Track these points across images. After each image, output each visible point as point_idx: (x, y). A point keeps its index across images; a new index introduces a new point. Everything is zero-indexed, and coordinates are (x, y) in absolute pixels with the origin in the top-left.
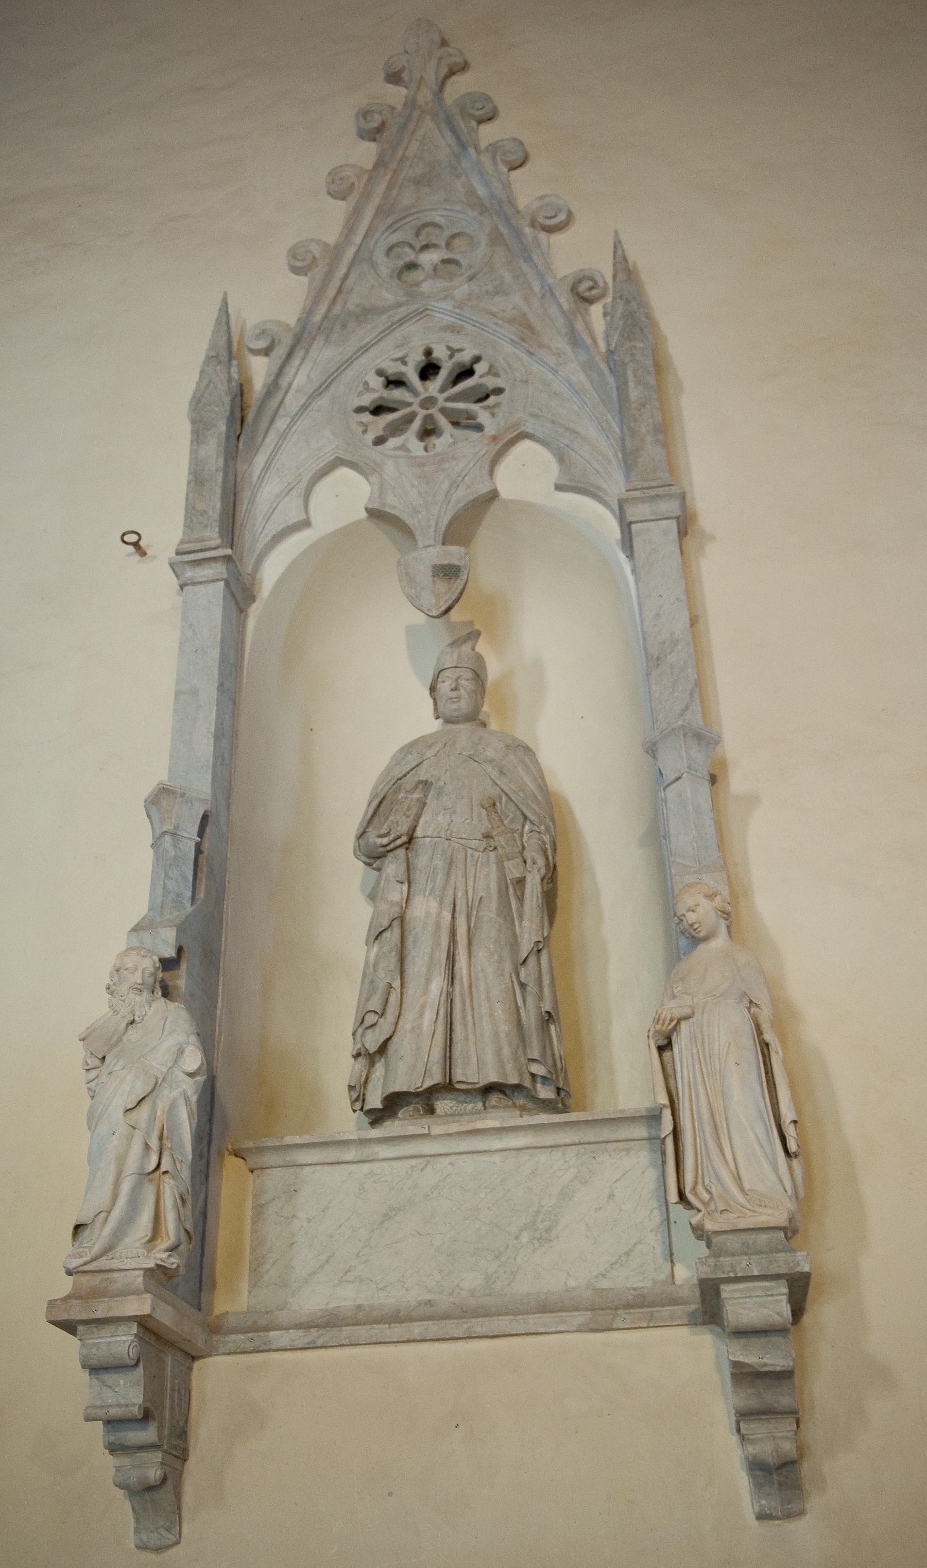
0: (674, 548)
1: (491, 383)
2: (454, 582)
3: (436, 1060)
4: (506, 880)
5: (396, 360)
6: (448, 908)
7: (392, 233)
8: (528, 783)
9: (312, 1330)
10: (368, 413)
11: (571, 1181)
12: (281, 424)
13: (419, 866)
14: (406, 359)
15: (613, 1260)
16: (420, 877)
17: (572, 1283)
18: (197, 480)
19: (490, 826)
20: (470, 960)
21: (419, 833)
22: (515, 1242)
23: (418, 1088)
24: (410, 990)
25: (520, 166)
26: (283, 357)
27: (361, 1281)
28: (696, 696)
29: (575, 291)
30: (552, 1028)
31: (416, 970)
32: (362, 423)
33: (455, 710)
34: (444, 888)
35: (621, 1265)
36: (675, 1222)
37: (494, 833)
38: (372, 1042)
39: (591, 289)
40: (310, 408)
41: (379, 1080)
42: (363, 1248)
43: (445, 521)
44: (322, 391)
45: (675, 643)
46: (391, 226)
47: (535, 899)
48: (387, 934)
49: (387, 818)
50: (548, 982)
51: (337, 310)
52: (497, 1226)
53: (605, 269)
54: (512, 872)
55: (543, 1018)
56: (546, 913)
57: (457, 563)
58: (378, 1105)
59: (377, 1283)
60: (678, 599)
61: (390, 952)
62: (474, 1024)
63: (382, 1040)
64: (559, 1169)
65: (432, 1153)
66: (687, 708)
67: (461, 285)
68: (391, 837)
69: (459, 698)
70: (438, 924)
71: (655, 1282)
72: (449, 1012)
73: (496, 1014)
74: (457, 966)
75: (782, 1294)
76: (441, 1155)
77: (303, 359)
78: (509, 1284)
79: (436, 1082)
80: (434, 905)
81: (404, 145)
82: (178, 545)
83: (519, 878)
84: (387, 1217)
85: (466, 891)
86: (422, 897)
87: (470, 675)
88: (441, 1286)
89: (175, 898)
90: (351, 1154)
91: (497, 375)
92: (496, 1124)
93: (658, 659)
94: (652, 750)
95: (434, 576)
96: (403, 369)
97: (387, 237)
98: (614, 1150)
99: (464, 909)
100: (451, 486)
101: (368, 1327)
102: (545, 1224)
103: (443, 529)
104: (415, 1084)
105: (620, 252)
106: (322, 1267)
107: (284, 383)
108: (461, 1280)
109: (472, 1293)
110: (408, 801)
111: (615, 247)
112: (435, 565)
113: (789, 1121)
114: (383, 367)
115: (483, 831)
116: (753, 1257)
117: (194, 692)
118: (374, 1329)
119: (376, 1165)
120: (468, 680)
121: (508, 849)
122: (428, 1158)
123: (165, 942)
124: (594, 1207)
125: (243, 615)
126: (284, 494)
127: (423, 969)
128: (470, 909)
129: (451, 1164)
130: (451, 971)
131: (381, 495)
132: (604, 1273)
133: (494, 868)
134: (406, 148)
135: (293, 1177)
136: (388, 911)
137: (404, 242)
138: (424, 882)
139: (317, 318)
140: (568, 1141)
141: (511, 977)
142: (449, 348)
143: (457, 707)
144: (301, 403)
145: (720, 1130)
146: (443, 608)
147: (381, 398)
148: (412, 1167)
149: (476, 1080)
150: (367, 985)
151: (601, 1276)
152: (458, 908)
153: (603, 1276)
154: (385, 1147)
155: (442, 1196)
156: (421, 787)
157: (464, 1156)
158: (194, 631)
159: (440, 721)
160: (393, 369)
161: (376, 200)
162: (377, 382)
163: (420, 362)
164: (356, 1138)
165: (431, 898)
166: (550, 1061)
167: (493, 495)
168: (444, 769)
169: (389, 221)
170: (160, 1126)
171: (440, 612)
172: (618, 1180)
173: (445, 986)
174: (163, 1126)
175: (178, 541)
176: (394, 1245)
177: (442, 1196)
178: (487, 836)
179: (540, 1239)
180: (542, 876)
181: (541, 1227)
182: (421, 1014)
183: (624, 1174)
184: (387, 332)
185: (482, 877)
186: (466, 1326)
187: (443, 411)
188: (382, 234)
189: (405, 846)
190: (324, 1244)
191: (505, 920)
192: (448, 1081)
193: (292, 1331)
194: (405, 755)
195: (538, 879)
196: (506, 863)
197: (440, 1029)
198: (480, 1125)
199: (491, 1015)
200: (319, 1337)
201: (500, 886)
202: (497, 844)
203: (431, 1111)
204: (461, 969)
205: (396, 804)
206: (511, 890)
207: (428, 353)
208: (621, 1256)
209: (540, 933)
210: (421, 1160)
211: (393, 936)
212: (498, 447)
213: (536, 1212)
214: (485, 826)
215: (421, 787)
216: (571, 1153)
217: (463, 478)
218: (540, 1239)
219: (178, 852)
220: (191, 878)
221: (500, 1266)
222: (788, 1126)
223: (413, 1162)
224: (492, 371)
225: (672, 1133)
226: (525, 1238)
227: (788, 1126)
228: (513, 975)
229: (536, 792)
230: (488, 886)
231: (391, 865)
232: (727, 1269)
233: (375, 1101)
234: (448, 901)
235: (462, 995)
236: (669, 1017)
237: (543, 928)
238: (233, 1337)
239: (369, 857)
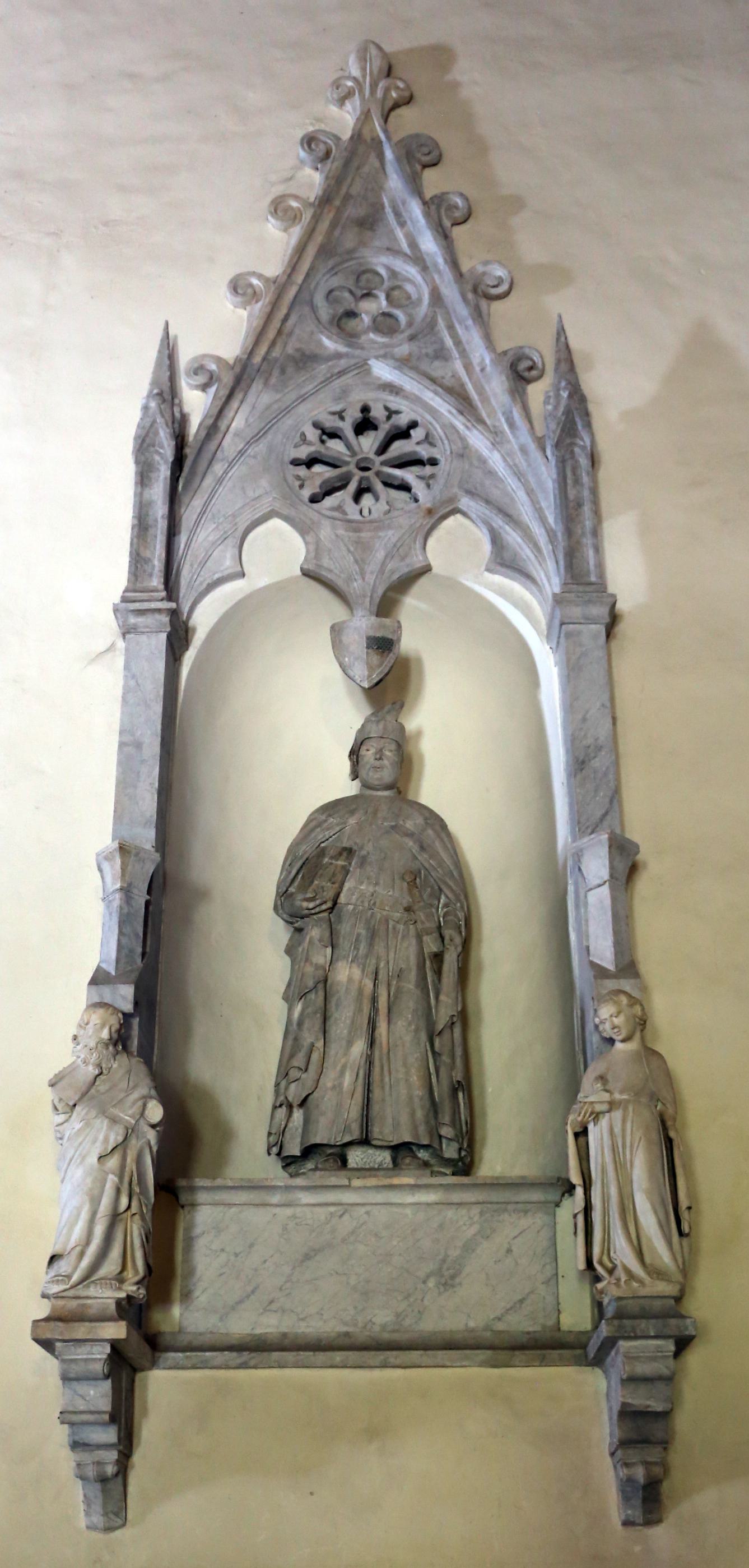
0: (601, 653)
1: (424, 452)
2: (388, 656)
4: (423, 953)
5: (333, 413)
7: (333, 275)
8: (446, 860)
9: (244, 1353)
10: (304, 466)
12: (218, 468)
13: (343, 932)
14: (343, 414)
15: (508, 1306)
16: (345, 944)
17: (472, 1324)
18: (142, 526)
19: (411, 900)
20: (389, 1027)
21: (342, 899)
22: (423, 1286)
24: (333, 1049)
25: (465, 222)
26: (223, 399)
27: (284, 1311)
29: (514, 368)
30: (460, 1095)
31: (338, 1031)
32: (298, 476)
33: (378, 779)
36: (563, 1276)
37: (416, 907)
38: (294, 1093)
39: (531, 368)
40: (246, 454)
41: (297, 1129)
42: (286, 1282)
43: (380, 591)
44: (260, 437)
45: (599, 748)
46: (332, 268)
47: (452, 975)
49: (312, 882)
51: (276, 353)
53: (546, 353)
54: (430, 947)
55: (454, 1086)
57: (390, 636)
58: (297, 1152)
59: (298, 1315)
60: (603, 705)
61: (315, 1013)
63: (304, 1096)
64: (465, 1225)
67: (401, 345)
68: (318, 902)
71: (544, 1326)
74: (377, 1032)
75: (670, 1352)
76: (358, 1204)
77: (242, 402)
78: (416, 1322)
80: (357, 973)
81: (349, 180)
82: (124, 592)
84: (307, 1257)
86: (345, 962)
87: (393, 747)
90: (276, 1198)
91: (432, 445)
92: (411, 1181)
95: (368, 648)
96: (340, 424)
97: (327, 280)
100: (386, 557)
103: (378, 600)
104: (335, 1139)
105: (563, 339)
106: (248, 1297)
107: (223, 426)
108: (374, 1316)
109: (384, 1327)
111: (558, 334)
114: (320, 419)
115: (405, 905)
121: (428, 925)
122: (346, 1207)
123: (124, 998)
126: (220, 542)
129: (367, 1213)
131: (318, 555)
132: (500, 1316)
133: (414, 941)
134: (351, 185)
135: (222, 1214)
137: (344, 287)
139: (257, 359)
140: (473, 1200)
141: (426, 1046)
142: (387, 408)
143: (379, 776)
144: (240, 448)
147: (316, 452)
148: (331, 1213)
149: (391, 1139)
150: (290, 1042)
152: (380, 977)
154: (307, 1194)
156: (345, 854)
157: (379, 1207)
158: (137, 681)
160: (331, 423)
161: (319, 238)
162: (312, 434)
163: (356, 419)
165: (354, 965)
166: (458, 1127)
167: (427, 569)
169: (331, 263)
174: (132, 1172)
175: (123, 588)
178: (408, 909)
179: (445, 1284)
182: (342, 1073)
184: (327, 382)
186: (382, 1357)
187: (378, 474)
188: (324, 275)
189: (329, 911)
190: (250, 1277)
192: (364, 1137)
195: (455, 956)
196: (425, 938)
197: (360, 1090)
200: (250, 1359)
203: (344, 1162)
206: (428, 963)
207: (365, 409)
209: (455, 1008)
210: (340, 1208)
211: (317, 998)
212: (433, 520)
214: (406, 900)
215: (345, 854)
216: (475, 1211)
217: (398, 549)
218: (445, 1284)
220: (141, 935)
223: (332, 1209)
224: (428, 439)
225: (583, 1212)
226: (431, 1283)
228: (428, 1044)
231: (315, 928)
233: (294, 1149)
234: (371, 969)
235: (381, 1059)
236: (590, 1110)
237: (457, 1004)
238: (172, 1355)
239: (291, 916)
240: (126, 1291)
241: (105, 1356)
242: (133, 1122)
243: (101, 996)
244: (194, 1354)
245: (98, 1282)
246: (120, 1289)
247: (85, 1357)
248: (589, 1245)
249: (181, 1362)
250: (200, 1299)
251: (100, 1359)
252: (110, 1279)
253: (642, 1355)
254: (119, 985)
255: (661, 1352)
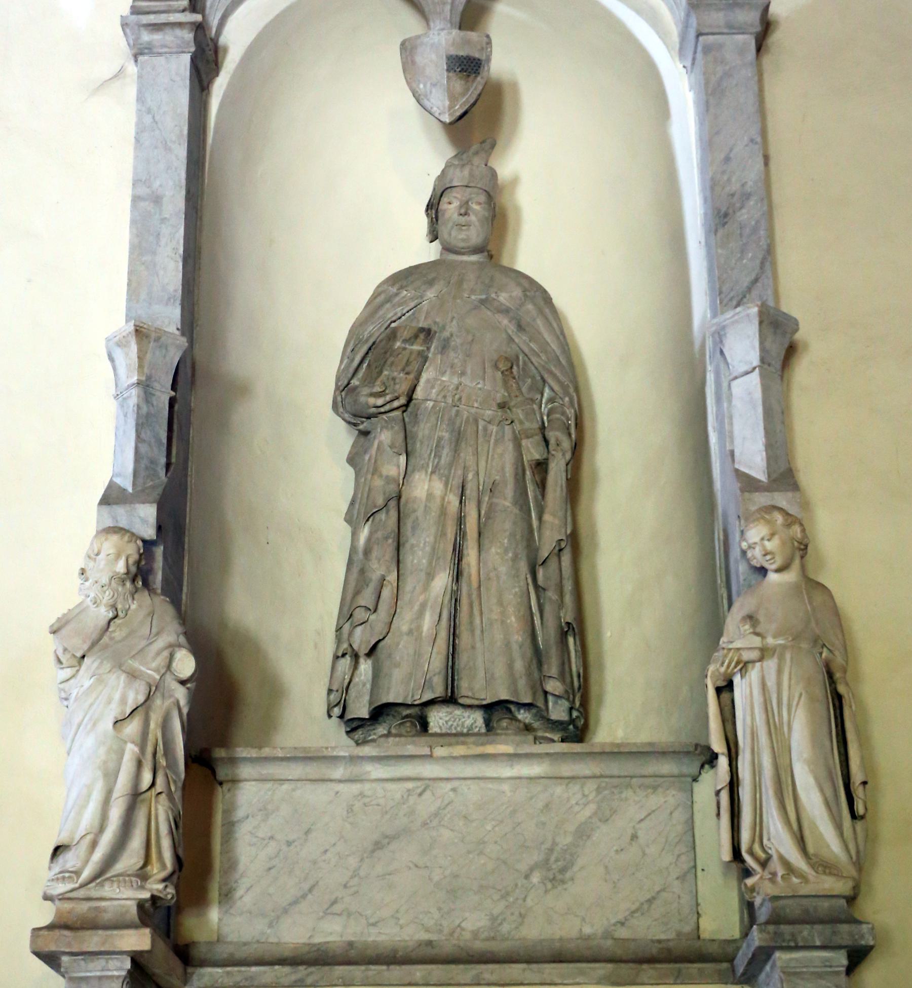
0: (749, 72)
2: (473, 81)
3: (437, 670)
6: (457, 491)
11: (590, 817)
13: (420, 435)
15: (634, 907)
16: (422, 450)
17: (587, 930)
19: (506, 394)
21: (419, 393)
22: (525, 881)
23: (415, 701)
24: (410, 584)
27: (349, 915)
28: (767, 264)
30: (571, 640)
31: (415, 561)
33: (463, 240)
34: (451, 465)
35: (642, 914)
38: (361, 639)
41: (364, 685)
45: (747, 196)
47: (559, 489)
48: (382, 516)
49: (380, 372)
50: (570, 588)
52: (505, 862)
55: (562, 628)
56: (569, 507)
57: (477, 55)
60: (752, 140)
61: (386, 538)
62: (482, 631)
63: (373, 643)
65: (432, 776)
66: (756, 280)
68: (388, 398)
69: (468, 225)
70: (443, 512)
71: (679, 934)
72: (453, 614)
73: (509, 621)
74: (464, 561)
76: (441, 779)
78: (517, 928)
79: (437, 695)
80: (438, 487)
83: (538, 460)
84: (378, 846)
85: (478, 474)
87: (482, 198)
88: (441, 925)
89: (149, 465)
90: (339, 772)
93: (726, 215)
94: (719, 333)
95: (448, 70)
98: (640, 787)
99: (475, 494)
101: (363, 968)
102: (559, 863)
104: (413, 696)
106: (304, 896)
109: (475, 934)
110: (406, 353)
112: (451, 56)
113: (859, 782)
116: (816, 926)
117: (157, 200)
118: (371, 970)
119: (367, 786)
120: (480, 204)
122: (427, 782)
123: (144, 521)
124: (615, 848)
125: (204, 93)
127: (424, 561)
128: (480, 494)
129: (454, 790)
130: (456, 566)
132: (623, 920)
133: (510, 446)
135: (270, 793)
136: (380, 489)
138: (426, 456)
140: (588, 772)
145: (784, 786)
146: (458, 114)
148: (409, 790)
151: (619, 925)
152: (468, 492)
153: (622, 924)
154: (377, 766)
155: (443, 826)
156: (422, 336)
157: (469, 782)
159: (436, 245)
164: (347, 754)
165: (435, 477)
166: (568, 680)
168: (450, 315)
170: (154, 741)
171: (454, 118)
172: (642, 820)
173: (450, 583)
174: (157, 740)
176: (387, 877)
177: (443, 826)
178: (502, 406)
180: (567, 461)
181: (554, 866)
182: (420, 614)
183: (649, 814)
185: (496, 456)
191: (521, 510)
193: (277, 967)
194: (398, 289)
195: (562, 464)
196: (524, 442)
197: (443, 634)
198: (490, 749)
199: (503, 622)
200: (308, 975)
201: (517, 468)
202: (514, 417)
203: (424, 725)
204: (469, 565)
205: (391, 355)
206: (528, 473)
208: (642, 904)
209: (563, 530)
210: (419, 783)
211: (389, 519)
213: (549, 849)
214: (501, 395)
215: (422, 336)
216: (591, 786)
219: (151, 408)
220: (165, 441)
221: (507, 907)
222: (858, 787)
223: (410, 785)
225: (728, 788)
226: (535, 878)
227: (858, 787)
228: (528, 576)
229: (558, 352)
230: (503, 468)
232: (787, 937)
233: (361, 709)
234: (456, 482)
235: (470, 596)
236: (736, 659)
238: (209, 970)
239: (355, 416)
240: (150, 890)
241: (124, 973)
242: (158, 677)
243: (114, 518)
244: (236, 969)
245: (115, 879)
246: (142, 888)
247: (98, 974)
248: (736, 828)
249: (220, 981)
250: (244, 899)
251: (118, 977)
252: (129, 876)
253: (804, 970)
254: (137, 505)
255: (831, 967)
